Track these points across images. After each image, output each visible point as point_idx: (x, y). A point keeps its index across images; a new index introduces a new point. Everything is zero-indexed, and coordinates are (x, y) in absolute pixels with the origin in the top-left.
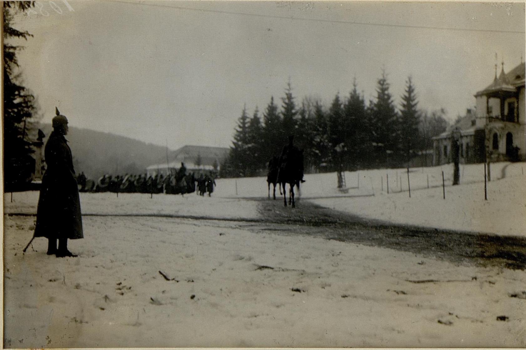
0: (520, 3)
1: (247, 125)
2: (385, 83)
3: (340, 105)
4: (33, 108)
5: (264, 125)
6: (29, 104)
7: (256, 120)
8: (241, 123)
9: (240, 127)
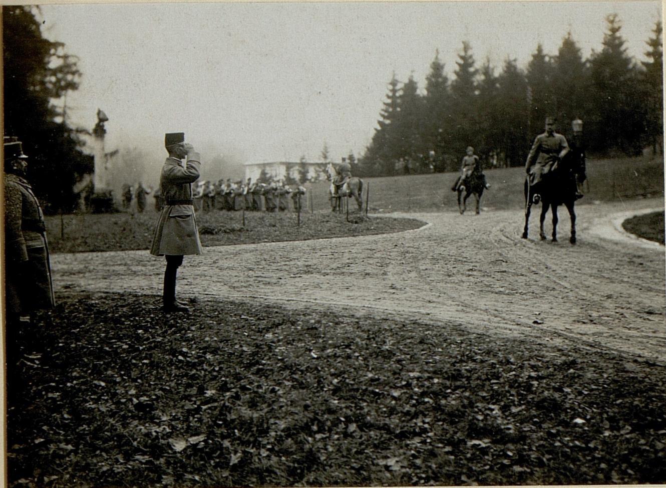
0: (166, 138)
1: (397, 94)
2: (617, 19)
3: (544, 57)
4: (80, 75)
5: (425, 92)
6: (74, 69)
7: (411, 86)
8: (391, 91)
9: (388, 97)
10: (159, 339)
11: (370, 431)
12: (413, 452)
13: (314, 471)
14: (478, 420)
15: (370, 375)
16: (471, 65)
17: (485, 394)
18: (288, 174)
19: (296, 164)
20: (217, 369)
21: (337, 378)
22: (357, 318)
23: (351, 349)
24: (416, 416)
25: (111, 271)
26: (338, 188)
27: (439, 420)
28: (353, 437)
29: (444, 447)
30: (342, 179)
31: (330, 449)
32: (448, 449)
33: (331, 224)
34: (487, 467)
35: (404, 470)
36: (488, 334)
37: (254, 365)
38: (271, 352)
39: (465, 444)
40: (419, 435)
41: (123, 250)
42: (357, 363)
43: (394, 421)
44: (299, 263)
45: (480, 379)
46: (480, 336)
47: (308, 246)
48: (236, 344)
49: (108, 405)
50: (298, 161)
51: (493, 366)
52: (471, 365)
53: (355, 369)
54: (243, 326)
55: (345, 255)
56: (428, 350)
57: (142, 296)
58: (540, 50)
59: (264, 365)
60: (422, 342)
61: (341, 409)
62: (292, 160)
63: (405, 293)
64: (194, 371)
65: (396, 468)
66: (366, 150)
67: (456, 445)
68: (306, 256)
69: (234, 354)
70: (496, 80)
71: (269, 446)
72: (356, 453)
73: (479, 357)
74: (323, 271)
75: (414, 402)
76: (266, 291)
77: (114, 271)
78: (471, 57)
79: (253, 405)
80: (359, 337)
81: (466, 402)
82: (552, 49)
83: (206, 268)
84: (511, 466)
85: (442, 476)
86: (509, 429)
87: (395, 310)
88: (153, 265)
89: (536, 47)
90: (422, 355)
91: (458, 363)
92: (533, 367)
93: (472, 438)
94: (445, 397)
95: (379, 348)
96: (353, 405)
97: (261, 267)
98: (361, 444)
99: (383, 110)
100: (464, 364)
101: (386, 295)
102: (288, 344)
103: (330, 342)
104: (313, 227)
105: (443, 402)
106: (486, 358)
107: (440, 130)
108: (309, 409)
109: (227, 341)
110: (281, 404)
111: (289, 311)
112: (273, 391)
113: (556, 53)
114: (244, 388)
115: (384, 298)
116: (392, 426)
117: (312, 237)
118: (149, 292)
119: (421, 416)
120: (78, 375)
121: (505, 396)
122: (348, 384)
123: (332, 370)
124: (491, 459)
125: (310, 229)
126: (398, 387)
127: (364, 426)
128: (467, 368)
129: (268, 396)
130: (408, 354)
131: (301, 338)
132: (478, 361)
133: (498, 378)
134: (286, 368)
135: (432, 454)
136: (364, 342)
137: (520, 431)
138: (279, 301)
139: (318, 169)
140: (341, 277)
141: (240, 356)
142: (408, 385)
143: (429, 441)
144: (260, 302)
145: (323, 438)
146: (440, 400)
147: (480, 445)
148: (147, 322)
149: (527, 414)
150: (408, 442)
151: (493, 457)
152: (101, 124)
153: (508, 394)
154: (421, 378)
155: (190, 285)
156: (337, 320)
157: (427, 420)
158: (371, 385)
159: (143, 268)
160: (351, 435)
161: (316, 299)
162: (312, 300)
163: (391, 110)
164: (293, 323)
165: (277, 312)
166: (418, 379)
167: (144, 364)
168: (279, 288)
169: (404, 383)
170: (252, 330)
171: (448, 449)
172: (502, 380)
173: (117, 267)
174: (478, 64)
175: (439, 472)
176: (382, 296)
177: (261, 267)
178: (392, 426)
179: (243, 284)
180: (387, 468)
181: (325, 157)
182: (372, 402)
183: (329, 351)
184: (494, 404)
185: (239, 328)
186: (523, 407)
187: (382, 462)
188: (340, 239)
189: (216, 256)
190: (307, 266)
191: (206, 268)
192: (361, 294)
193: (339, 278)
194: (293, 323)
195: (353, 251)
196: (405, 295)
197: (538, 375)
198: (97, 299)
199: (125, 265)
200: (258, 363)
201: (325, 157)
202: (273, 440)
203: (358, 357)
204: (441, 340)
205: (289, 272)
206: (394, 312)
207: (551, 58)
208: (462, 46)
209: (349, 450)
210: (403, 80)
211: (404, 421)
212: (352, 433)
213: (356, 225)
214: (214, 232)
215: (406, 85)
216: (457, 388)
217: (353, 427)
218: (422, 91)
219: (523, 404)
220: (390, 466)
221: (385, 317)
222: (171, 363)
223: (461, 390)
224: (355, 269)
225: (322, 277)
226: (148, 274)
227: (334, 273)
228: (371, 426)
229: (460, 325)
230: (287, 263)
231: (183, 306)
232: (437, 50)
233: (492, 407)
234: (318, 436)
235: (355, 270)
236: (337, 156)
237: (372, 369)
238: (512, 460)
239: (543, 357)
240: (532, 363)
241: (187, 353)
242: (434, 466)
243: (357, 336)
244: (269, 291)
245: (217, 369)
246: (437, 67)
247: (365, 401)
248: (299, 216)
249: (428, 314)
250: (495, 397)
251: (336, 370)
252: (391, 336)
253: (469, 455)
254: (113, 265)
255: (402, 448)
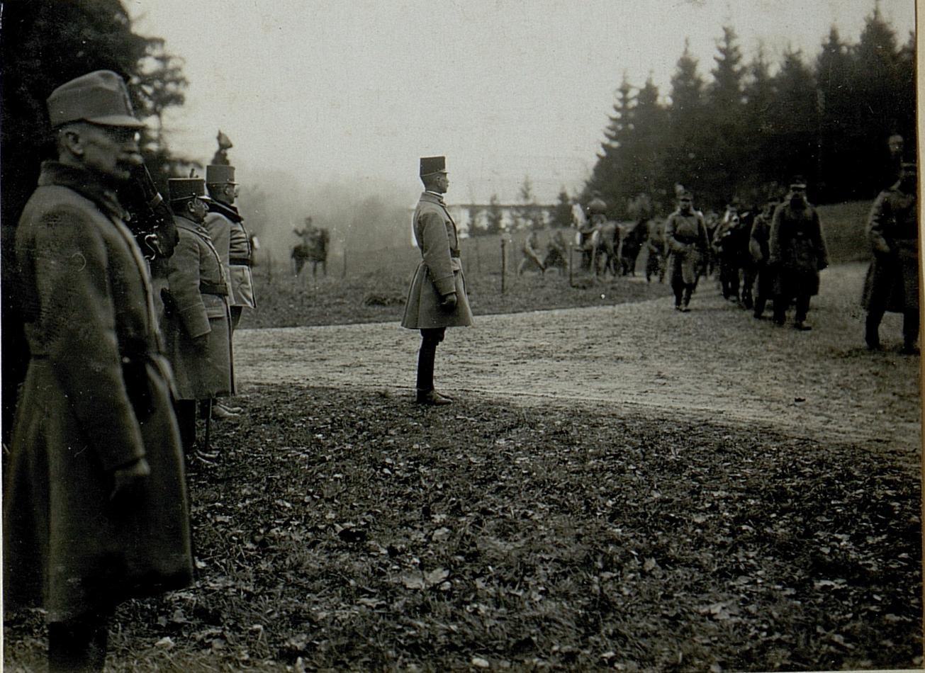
0: (439, 158)
5: (669, 101)
7: (649, 93)
9: (617, 109)
10: (349, 446)
11: (675, 568)
12: (742, 596)
13: (610, 621)
14: (823, 553)
15: (656, 495)
16: (735, 61)
17: (825, 520)
18: (473, 222)
19: (483, 207)
20: (440, 486)
21: (611, 498)
22: (621, 419)
23: (622, 460)
24: (734, 549)
25: (256, 355)
26: (585, 237)
27: (768, 554)
28: (653, 576)
29: (783, 590)
30: (591, 225)
31: (626, 593)
32: (790, 591)
33: (548, 290)
34: (850, 616)
35: (734, 620)
36: (814, 438)
37: (491, 480)
38: (510, 464)
39: (812, 585)
40: (745, 573)
41: (261, 327)
42: (634, 479)
43: (706, 556)
44: (518, 344)
45: (816, 500)
46: (804, 441)
47: (523, 321)
48: (458, 453)
49: (302, 532)
50: (487, 203)
51: (829, 482)
52: (798, 481)
53: (633, 486)
54: (462, 430)
55: (580, 332)
56: (733, 461)
57: (308, 388)
58: (834, 36)
59: (504, 481)
60: (721, 450)
61: (627, 540)
62: (478, 202)
63: (681, 384)
64: (410, 490)
65: (724, 616)
66: (584, 185)
67: (802, 589)
68: (525, 335)
69: (458, 466)
70: (772, 82)
71: (542, 588)
72: (663, 596)
73: (807, 469)
74: (554, 355)
75: (727, 530)
76: (481, 382)
77: (260, 355)
78: (736, 49)
79: (503, 534)
80: (631, 444)
81: (801, 530)
82: (852, 34)
83: (388, 351)
84: (882, 614)
85: (789, 626)
86: (870, 566)
87: (671, 407)
88: (312, 348)
89: (828, 33)
90: (726, 467)
91: (779, 478)
92: (887, 482)
93: (819, 579)
94: (770, 525)
95: (662, 459)
96: (643, 535)
97: (464, 349)
98: (667, 586)
99: (609, 128)
100: (788, 480)
101: (653, 387)
102: (531, 453)
103: (590, 451)
104: (523, 295)
105: (768, 530)
106: (818, 471)
107: (692, 156)
108: (582, 539)
109: (444, 449)
110: (543, 533)
111: (521, 409)
112: (525, 516)
113: (856, 40)
114: (485, 512)
115: (652, 391)
116: (705, 562)
117: (524, 308)
118: (316, 384)
119: (740, 549)
120: (249, 493)
121: (855, 522)
122: (630, 507)
123: (602, 488)
124: (851, 605)
125: (520, 298)
126: (700, 511)
127: (665, 562)
128: (794, 484)
129: (520, 521)
130: (706, 467)
131: (548, 445)
132: (808, 475)
133: (841, 498)
134: (537, 485)
135: (770, 598)
136: (638, 451)
137: (887, 569)
138: (503, 396)
139: (515, 213)
140: (583, 362)
141: (468, 470)
142: (714, 508)
143: (759, 581)
144: (476, 396)
145: (612, 578)
146: (763, 528)
147: (832, 586)
148: (326, 423)
149: (892, 547)
150: (732, 583)
151: (853, 603)
152: (223, 152)
153: (859, 520)
154: (731, 498)
155: (372, 374)
156: (594, 421)
157: (751, 555)
158: (662, 508)
159: (301, 352)
160: (650, 574)
161: (555, 393)
162: (549, 395)
163: (620, 127)
164: (532, 426)
165: (504, 411)
166: (726, 499)
167: (336, 479)
168: (497, 378)
169: (708, 505)
170: (477, 435)
171: (790, 591)
172: (846, 501)
173: (263, 349)
174: (747, 60)
175: (784, 622)
176: (647, 388)
177: (464, 349)
178: (705, 562)
179: (445, 373)
180: (710, 616)
181: (526, 197)
182: (669, 530)
183: (592, 462)
184: (840, 533)
185: (456, 432)
186: (884, 537)
187: (704, 610)
188: (565, 312)
189: (397, 335)
190: (530, 348)
191: (388, 351)
192: (618, 385)
193: (579, 365)
194: (532, 426)
195: (590, 327)
196: (681, 387)
197: (898, 495)
198: (247, 392)
199: (273, 347)
200: (495, 478)
201: (526, 197)
202: (544, 580)
203: (634, 470)
204: (748, 446)
205: (508, 358)
206: (670, 410)
207: (849, 48)
208: (722, 34)
209: (651, 593)
210: (638, 84)
211: (720, 556)
212: (650, 571)
213: (584, 292)
214: (386, 302)
215: (642, 91)
216: (784, 511)
217: (651, 563)
218: (665, 98)
219: (884, 533)
220: (715, 614)
221: (660, 417)
222: (374, 479)
223: (791, 514)
224: (598, 351)
225: (555, 362)
226: (309, 359)
227: (571, 358)
228: (676, 562)
229: (771, 427)
230: (501, 344)
231: (443, 399)
232: (686, 41)
233: (840, 536)
234: (607, 575)
235: (600, 354)
236: (547, 196)
237: (658, 486)
238: (882, 607)
239: (900, 468)
240: (887, 477)
241: (392, 465)
242: (775, 614)
243: (626, 443)
244: (484, 381)
245: (440, 486)
246: (687, 66)
247: (660, 529)
248: (503, 281)
249: (722, 412)
250: (841, 524)
251: (607, 488)
252: (675, 442)
253: (820, 600)
254: (257, 347)
255: (724, 590)
